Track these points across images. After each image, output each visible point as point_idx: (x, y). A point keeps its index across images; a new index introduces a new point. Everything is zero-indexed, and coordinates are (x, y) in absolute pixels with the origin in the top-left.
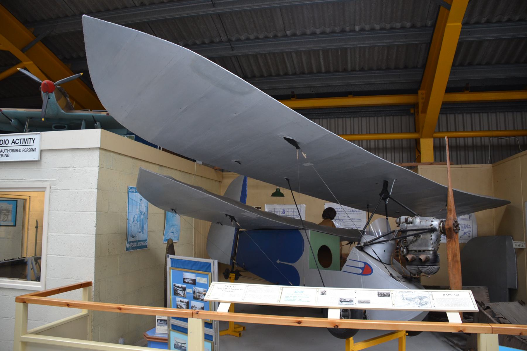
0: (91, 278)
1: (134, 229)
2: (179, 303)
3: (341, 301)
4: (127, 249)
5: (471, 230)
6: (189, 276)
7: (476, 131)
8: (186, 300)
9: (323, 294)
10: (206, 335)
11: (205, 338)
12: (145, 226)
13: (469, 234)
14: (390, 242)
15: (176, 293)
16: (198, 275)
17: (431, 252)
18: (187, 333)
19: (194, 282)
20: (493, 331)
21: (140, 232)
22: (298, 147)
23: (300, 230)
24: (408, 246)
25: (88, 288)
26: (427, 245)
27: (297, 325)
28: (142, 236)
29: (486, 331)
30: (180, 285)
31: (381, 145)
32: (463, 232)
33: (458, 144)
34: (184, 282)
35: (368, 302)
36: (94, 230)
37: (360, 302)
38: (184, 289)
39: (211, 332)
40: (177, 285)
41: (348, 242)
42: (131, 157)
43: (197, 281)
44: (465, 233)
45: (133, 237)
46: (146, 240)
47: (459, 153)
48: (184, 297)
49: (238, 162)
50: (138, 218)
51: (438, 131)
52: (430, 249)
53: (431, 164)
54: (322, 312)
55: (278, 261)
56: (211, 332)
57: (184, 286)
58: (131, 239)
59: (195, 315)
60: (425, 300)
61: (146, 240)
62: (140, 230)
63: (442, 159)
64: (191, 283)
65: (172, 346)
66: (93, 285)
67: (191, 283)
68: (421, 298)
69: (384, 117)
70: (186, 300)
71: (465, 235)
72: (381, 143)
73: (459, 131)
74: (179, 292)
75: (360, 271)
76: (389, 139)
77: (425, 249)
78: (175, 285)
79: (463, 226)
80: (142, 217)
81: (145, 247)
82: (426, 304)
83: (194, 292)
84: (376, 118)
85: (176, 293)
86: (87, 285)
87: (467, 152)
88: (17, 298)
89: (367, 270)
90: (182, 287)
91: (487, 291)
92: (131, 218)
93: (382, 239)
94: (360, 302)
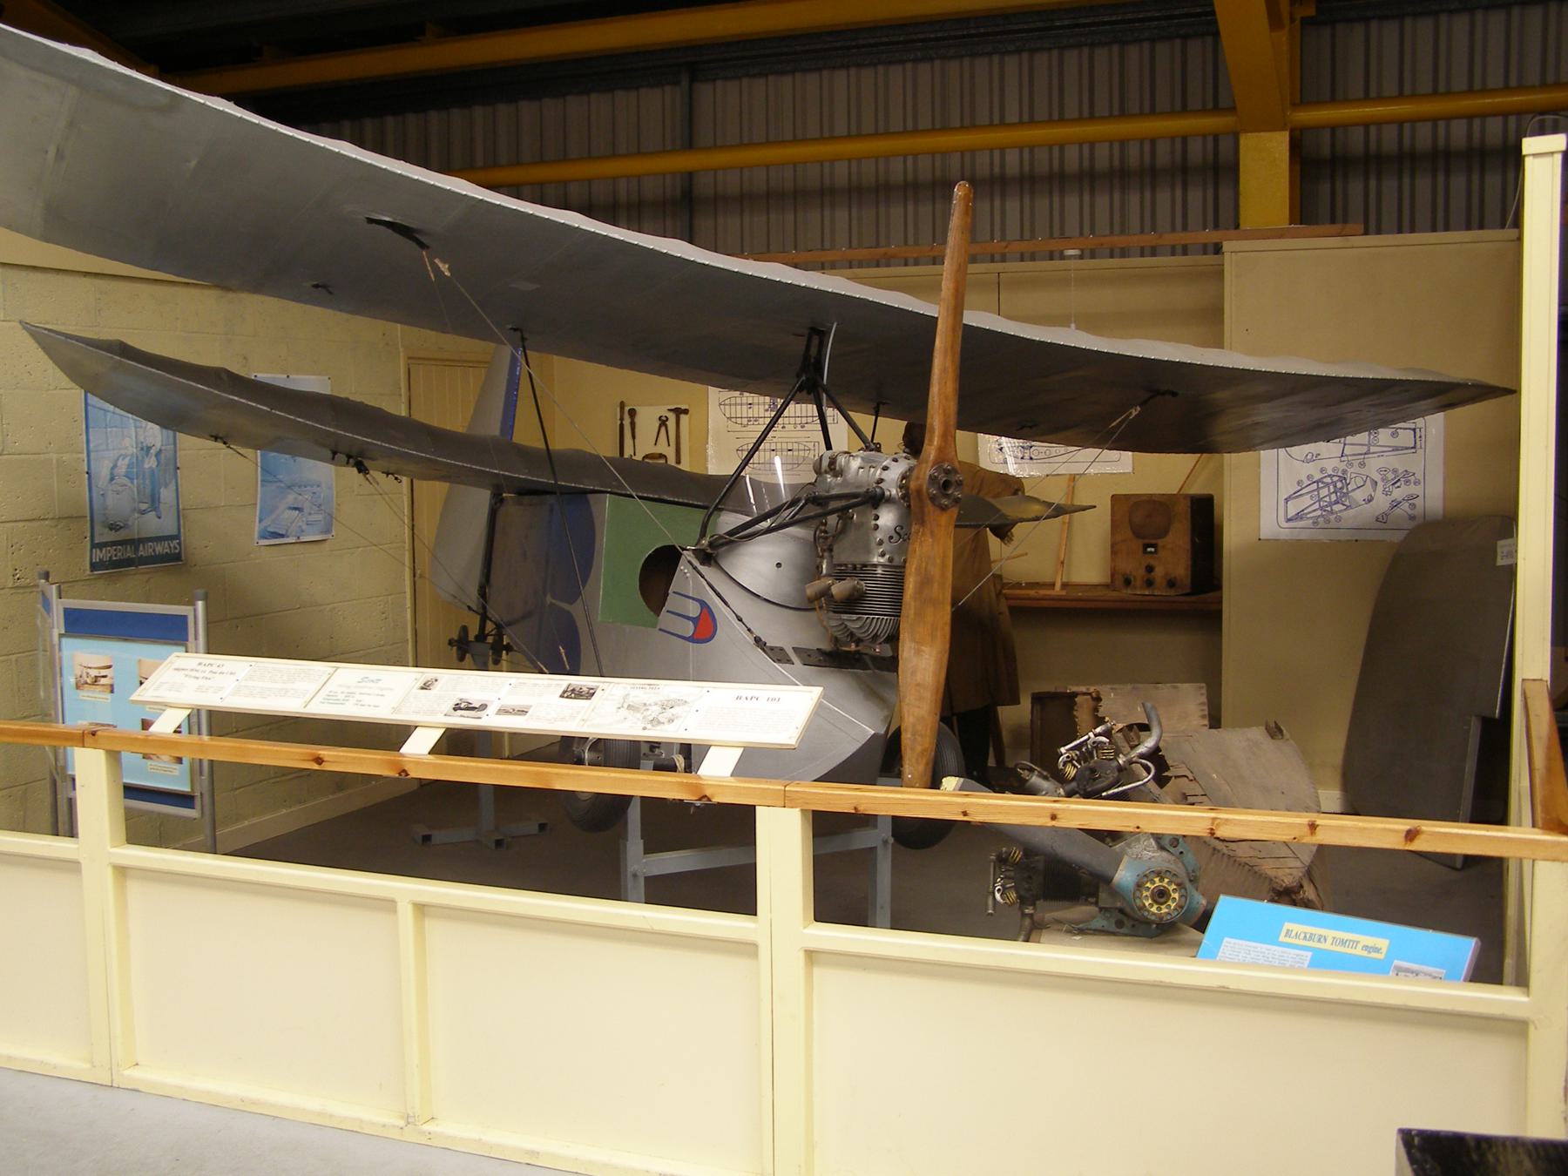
1: (118, 501)
3: (457, 708)
4: (94, 566)
5: (1417, 490)
7: (1415, 96)
9: (425, 687)
12: (167, 494)
13: (1413, 506)
17: (879, 571)
20: (786, 801)
21: (143, 513)
22: (422, 245)
24: (831, 550)
26: (869, 552)
27: (316, 767)
28: (152, 525)
31: (1102, 163)
32: (1390, 498)
33: (1373, 146)
35: (523, 712)
37: (503, 711)
42: (86, 274)
44: (1396, 504)
45: (113, 527)
46: (177, 537)
47: (1339, 185)
49: (324, 287)
50: (130, 466)
51: (1361, 94)
52: (876, 560)
53: (1279, 234)
54: (391, 736)
55: (549, 599)
58: (104, 535)
59: (88, 739)
61: (177, 537)
62: (144, 507)
63: (1339, 212)
68: (667, 706)
69: (1146, 46)
71: (1397, 511)
72: (1133, 152)
73: (1381, 99)
75: (690, 629)
79: (1390, 476)
80: (151, 463)
81: (176, 557)
82: (671, 721)
84: (1115, 48)
87: (1441, 178)
88: (875, 826)
89: (705, 627)
91: (1204, 699)
92: (103, 470)
94: (503, 711)
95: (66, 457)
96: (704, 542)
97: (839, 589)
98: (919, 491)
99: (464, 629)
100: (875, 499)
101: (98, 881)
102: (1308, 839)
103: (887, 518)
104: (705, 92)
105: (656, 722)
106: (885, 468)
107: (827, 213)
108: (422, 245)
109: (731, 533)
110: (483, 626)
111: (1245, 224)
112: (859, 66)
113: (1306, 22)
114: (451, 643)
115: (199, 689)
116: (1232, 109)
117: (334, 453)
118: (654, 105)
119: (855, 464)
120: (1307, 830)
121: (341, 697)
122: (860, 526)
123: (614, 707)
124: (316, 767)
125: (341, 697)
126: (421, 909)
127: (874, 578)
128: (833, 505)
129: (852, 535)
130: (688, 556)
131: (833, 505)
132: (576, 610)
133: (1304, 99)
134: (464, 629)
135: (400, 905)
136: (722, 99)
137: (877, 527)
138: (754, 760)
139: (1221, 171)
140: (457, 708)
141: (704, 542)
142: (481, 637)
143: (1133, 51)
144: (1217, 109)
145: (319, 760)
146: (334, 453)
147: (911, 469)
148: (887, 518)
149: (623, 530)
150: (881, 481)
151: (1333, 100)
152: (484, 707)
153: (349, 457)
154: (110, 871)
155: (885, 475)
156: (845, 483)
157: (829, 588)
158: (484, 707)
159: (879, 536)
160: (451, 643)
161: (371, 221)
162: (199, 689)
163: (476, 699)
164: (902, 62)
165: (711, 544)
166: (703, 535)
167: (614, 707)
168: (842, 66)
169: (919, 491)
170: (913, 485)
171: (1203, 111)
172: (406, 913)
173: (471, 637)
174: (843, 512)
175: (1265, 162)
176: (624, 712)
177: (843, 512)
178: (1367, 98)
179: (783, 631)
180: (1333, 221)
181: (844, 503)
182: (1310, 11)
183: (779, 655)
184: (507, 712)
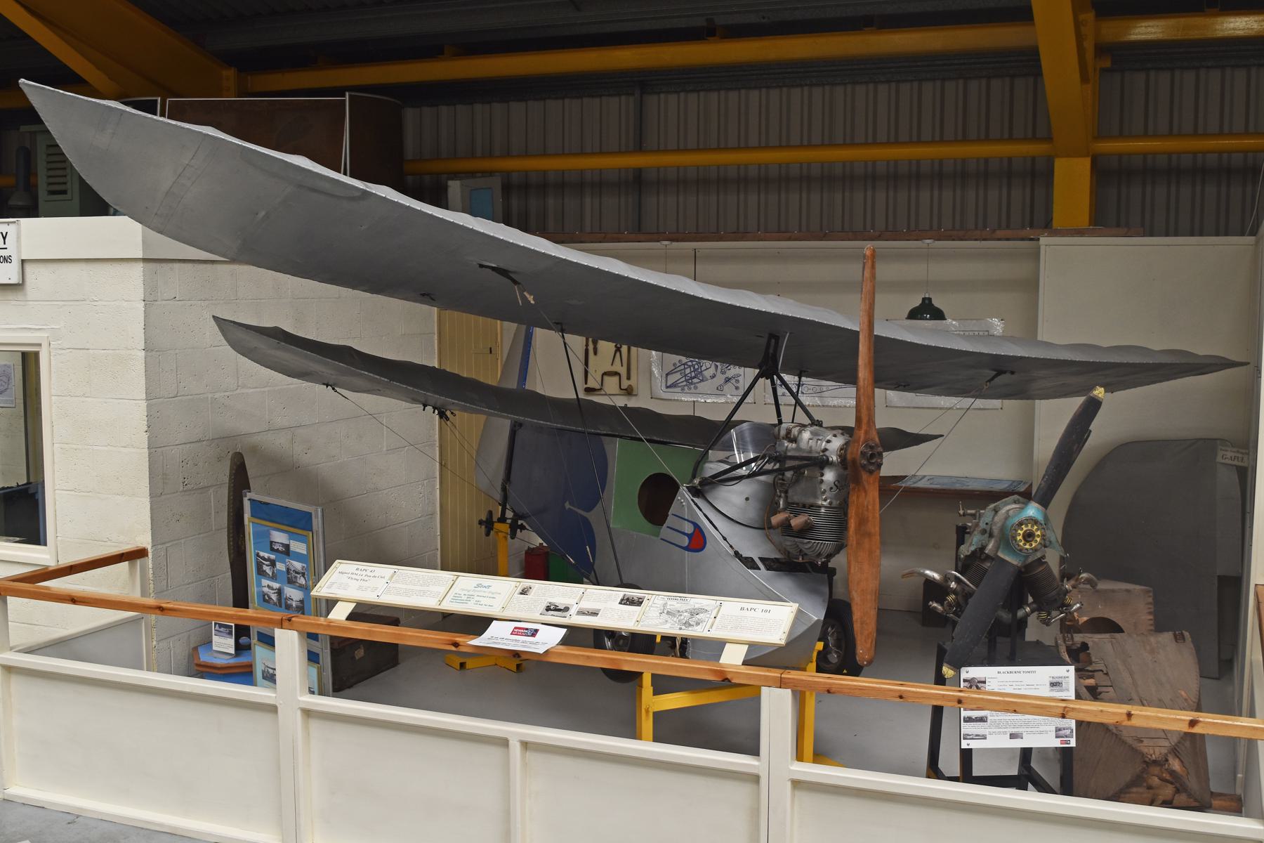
0: (144, 540)
2: (266, 590)
3: (548, 609)
6: (279, 537)
8: (276, 585)
9: (524, 592)
10: (310, 653)
11: (309, 659)
14: (762, 478)
15: (261, 572)
16: (292, 536)
18: (273, 646)
19: (287, 551)
20: (782, 684)
22: (515, 282)
23: (734, 419)
24: (786, 492)
25: (138, 562)
26: (816, 497)
29: (771, 683)
30: (266, 555)
34: (272, 550)
35: (595, 614)
36: (143, 439)
37: (581, 613)
38: (273, 563)
39: (316, 646)
40: (262, 554)
41: (893, 463)
43: (292, 548)
48: (274, 578)
53: (1080, 233)
55: (567, 505)
56: (316, 646)
57: (273, 557)
59: (286, 624)
60: (701, 616)
64: (281, 552)
65: (259, 674)
66: (150, 555)
67: (281, 552)
68: (694, 613)
70: (276, 585)
74: (265, 568)
76: (858, 144)
77: (811, 501)
78: (258, 555)
82: (698, 624)
83: (288, 570)
84: (961, 82)
85: (261, 572)
86: (140, 553)
90: (269, 560)
93: (744, 471)
95: (217, 396)
96: (696, 481)
97: (797, 522)
98: (854, 461)
99: (490, 513)
100: (821, 463)
101: (290, 719)
102: (1126, 723)
103: (829, 476)
104: (652, 100)
105: (688, 624)
106: (829, 441)
107: (742, 196)
108: (515, 282)
109: (714, 476)
110: (503, 512)
111: (1056, 224)
112: (768, 87)
113: (1103, 70)
114: (481, 522)
115: (360, 588)
116: (1049, 139)
117: (425, 406)
118: (616, 108)
119: (806, 435)
120: (1125, 717)
121: (464, 598)
122: (811, 478)
123: (656, 613)
124: (453, 648)
125: (464, 598)
126: (526, 745)
127: (818, 516)
128: (789, 463)
129: (803, 485)
130: (683, 490)
131: (789, 463)
132: (592, 516)
133: (1100, 136)
134: (490, 513)
135: (511, 742)
136: (668, 108)
137: (822, 481)
138: (760, 657)
139: (1039, 176)
140: (548, 609)
141: (696, 481)
142: (502, 519)
143: (974, 85)
144: (1034, 138)
145: (456, 644)
146: (425, 406)
147: (847, 444)
148: (829, 476)
149: (627, 466)
150: (826, 450)
151: (1121, 136)
152: (567, 609)
153: (435, 408)
154: (299, 713)
155: (829, 446)
156: (798, 449)
157: (788, 520)
158: (567, 609)
159: (823, 487)
160: (481, 522)
161: (481, 266)
162: (360, 588)
163: (560, 601)
164: (801, 86)
165: (701, 483)
166: (694, 477)
167: (656, 613)
168: (755, 88)
169: (854, 461)
170: (849, 457)
171: (1025, 139)
172: (515, 748)
173: (495, 519)
174: (797, 470)
175: (1073, 179)
176: (665, 616)
177: (797, 470)
178: (1145, 135)
179: (753, 546)
180: (1118, 226)
181: (796, 463)
182: (1108, 64)
183: (749, 563)
184: (584, 614)
